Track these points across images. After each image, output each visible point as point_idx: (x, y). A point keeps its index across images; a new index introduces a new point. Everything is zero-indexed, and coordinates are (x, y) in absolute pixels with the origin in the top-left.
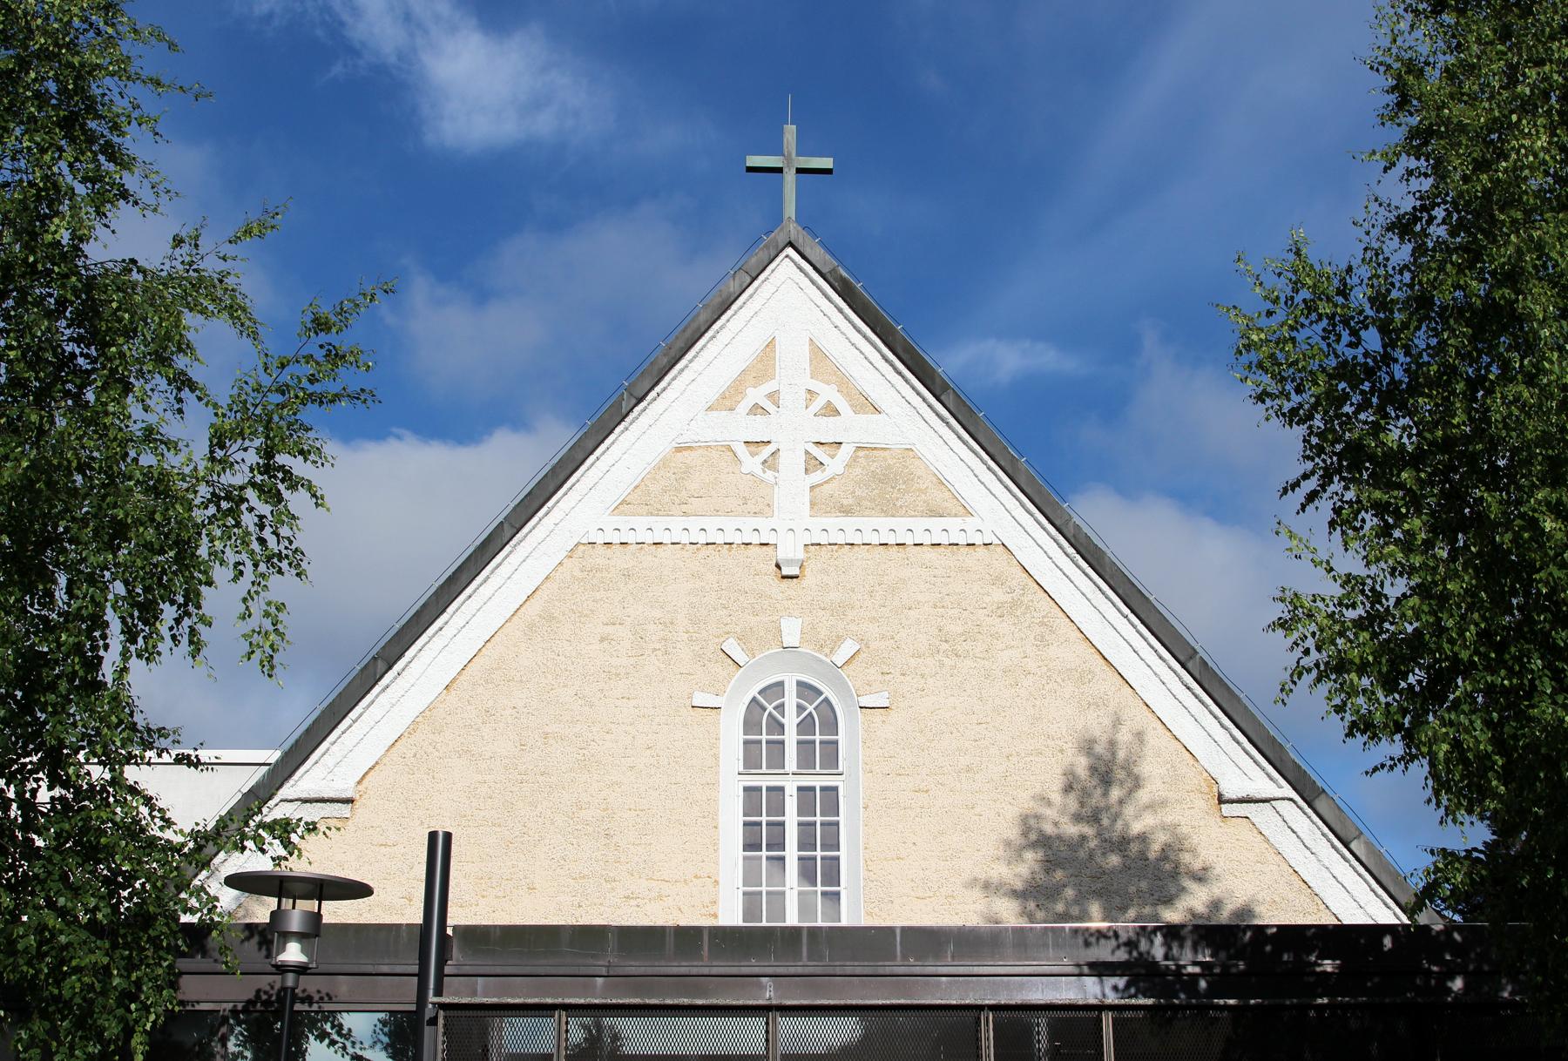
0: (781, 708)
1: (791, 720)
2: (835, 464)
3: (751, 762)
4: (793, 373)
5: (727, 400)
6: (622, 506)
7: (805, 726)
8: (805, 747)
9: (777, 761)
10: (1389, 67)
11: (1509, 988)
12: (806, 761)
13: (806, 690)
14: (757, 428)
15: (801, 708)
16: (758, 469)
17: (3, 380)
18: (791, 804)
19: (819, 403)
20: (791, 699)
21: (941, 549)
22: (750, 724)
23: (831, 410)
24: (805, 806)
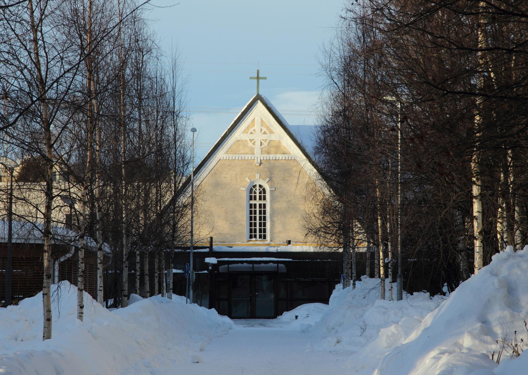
0: (256, 189)
4: (257, 127)
7: (260, 193)
8: (260, 197)
9: (260, 205)
10: (23, 142)
11: (477, 103)
12: (260, 199)
14: (252, 137)
15: (260, 189)
16: (252, 145)
18: (258, 197)
19: (263, 132)
20: (258, 188)
21: (295, 241)
23: (265, 133)
24: (255, 197)
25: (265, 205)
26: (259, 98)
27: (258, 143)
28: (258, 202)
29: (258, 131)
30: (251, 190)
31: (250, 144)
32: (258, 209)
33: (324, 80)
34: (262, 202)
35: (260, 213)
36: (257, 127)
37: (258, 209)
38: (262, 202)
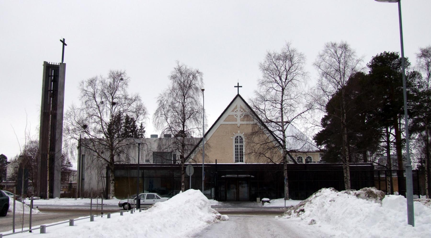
1: (239, 139)
2: (235, 117)
3: (236, 143)
4: (238, 109)
5: (233, 111)
6: (224, 121)
7: (240, 140)
8: (240, 142)
9: (240, 146)
13: (240, 137)
14: (236, 113)
17: (12, 153)
20: (239, 137)
22: (236, 140)
24: (238, 142)
25: (236, 143)
26: (238, 95)
27: (239, 116)
28: (239, 144)
29: (239, 110)
30: (236, 138)
31: (235, 117)
32: (239, 159)
33: (22, 149)
34: (237, 144)
35: (240, 149)
36: (238, 109)
37: (239, 159)
38: (237, 144)
